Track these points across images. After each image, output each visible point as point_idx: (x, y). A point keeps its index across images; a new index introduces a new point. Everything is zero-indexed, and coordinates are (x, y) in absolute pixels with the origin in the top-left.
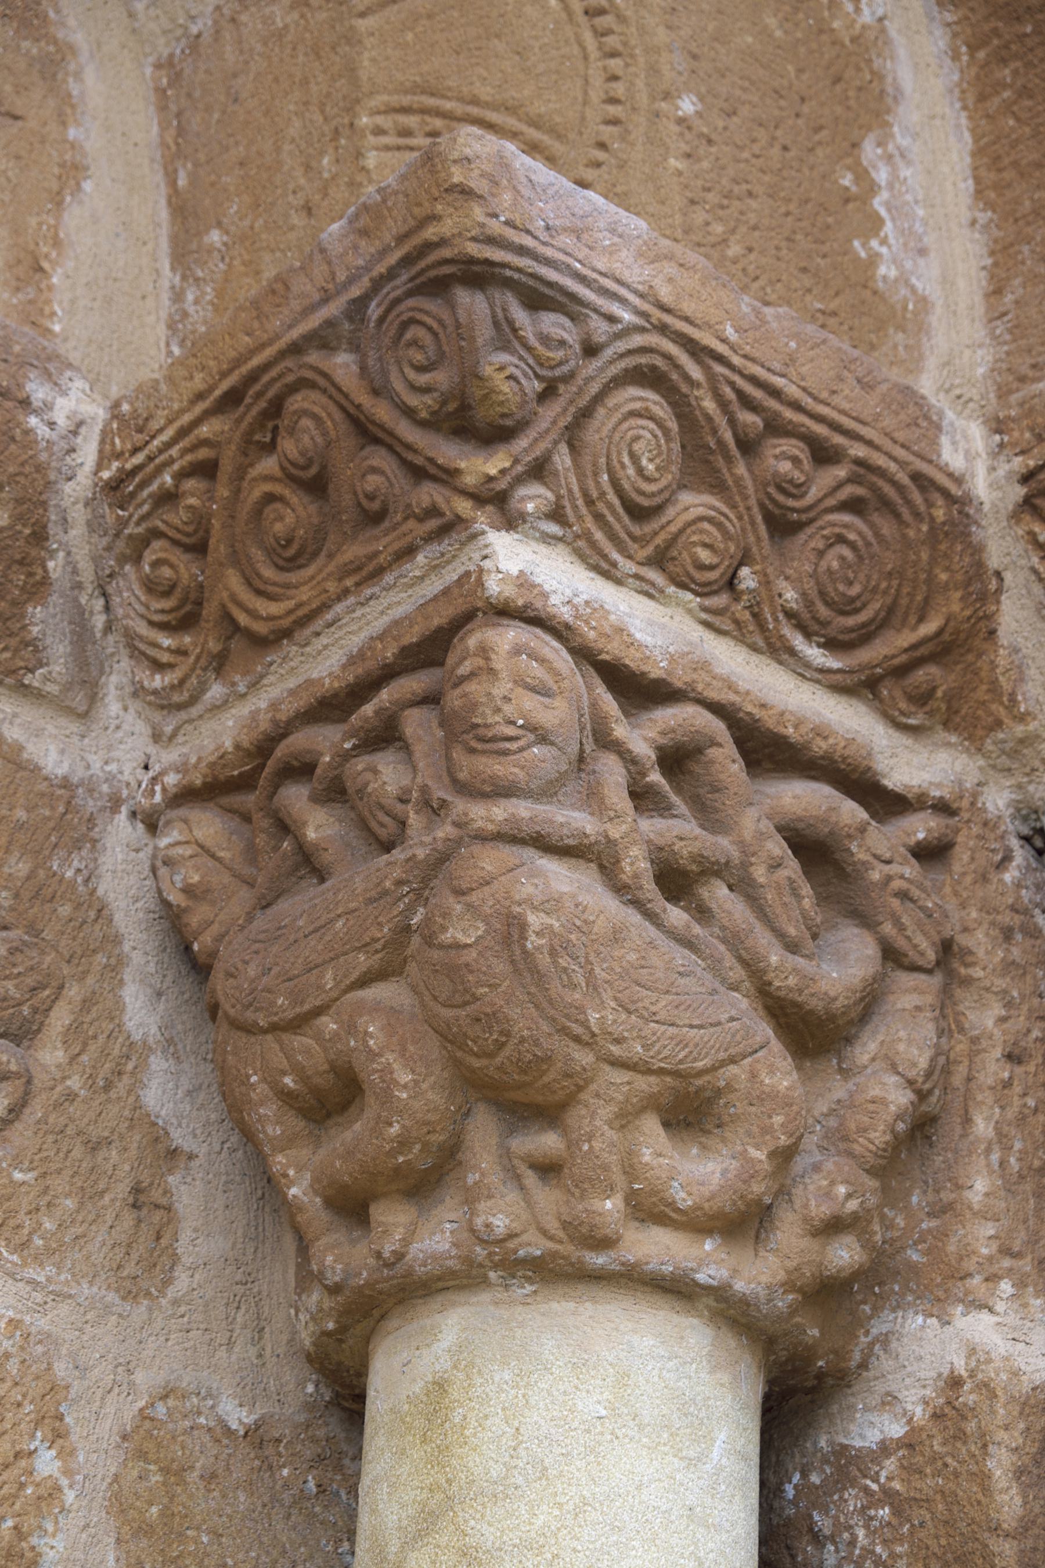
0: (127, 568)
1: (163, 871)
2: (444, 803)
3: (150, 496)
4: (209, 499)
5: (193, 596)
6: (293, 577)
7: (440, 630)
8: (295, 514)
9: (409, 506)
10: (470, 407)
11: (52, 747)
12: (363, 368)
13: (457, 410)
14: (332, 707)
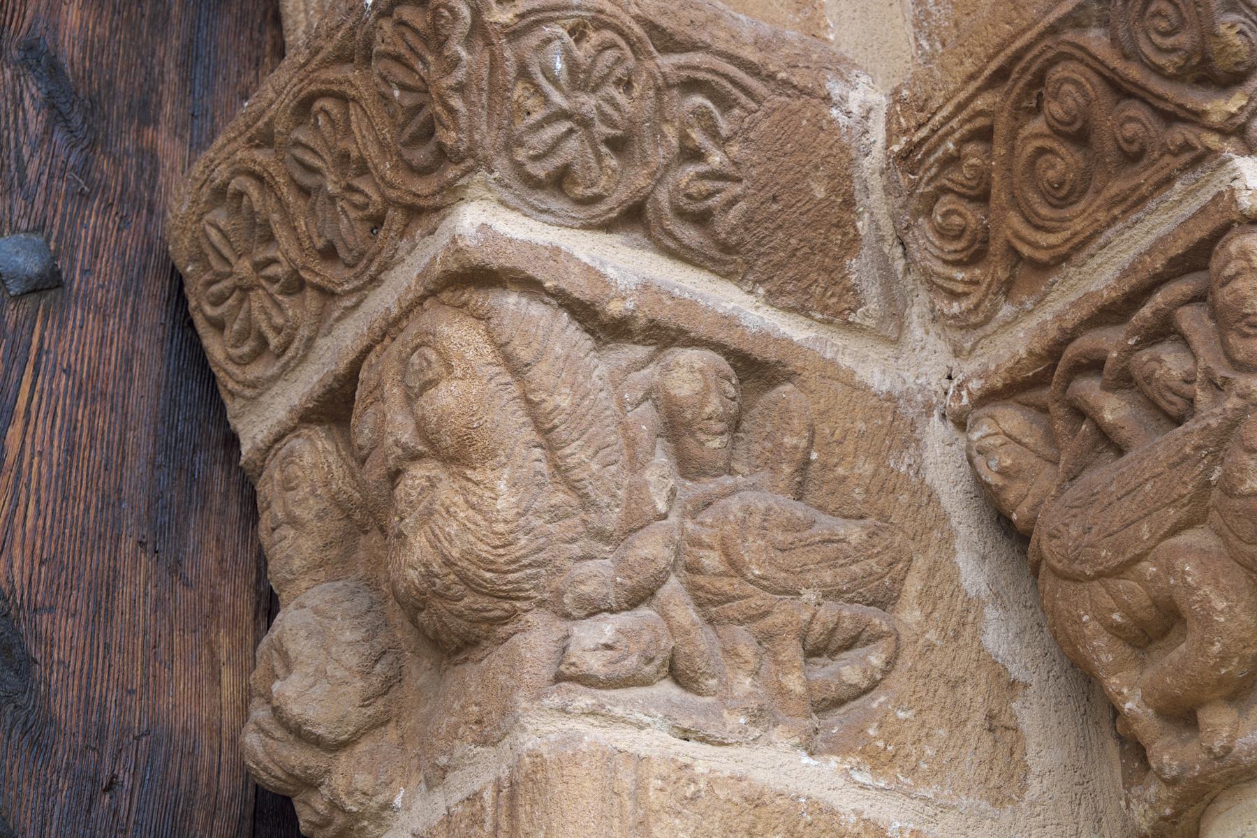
0: (921, 220)
1: (979, 460)
2: (1226, 380)
3: (936, 161)
4: (988, 158)
5: (980, 237)
6: (1066, 213)
7: (1202, 241)
8: (1064, 163)
9: (1164, 144)
10: (1210, 60)
11: (876, 370)
12: (1114, 40)
13: (1199, 63)
14: (1112, 313)
